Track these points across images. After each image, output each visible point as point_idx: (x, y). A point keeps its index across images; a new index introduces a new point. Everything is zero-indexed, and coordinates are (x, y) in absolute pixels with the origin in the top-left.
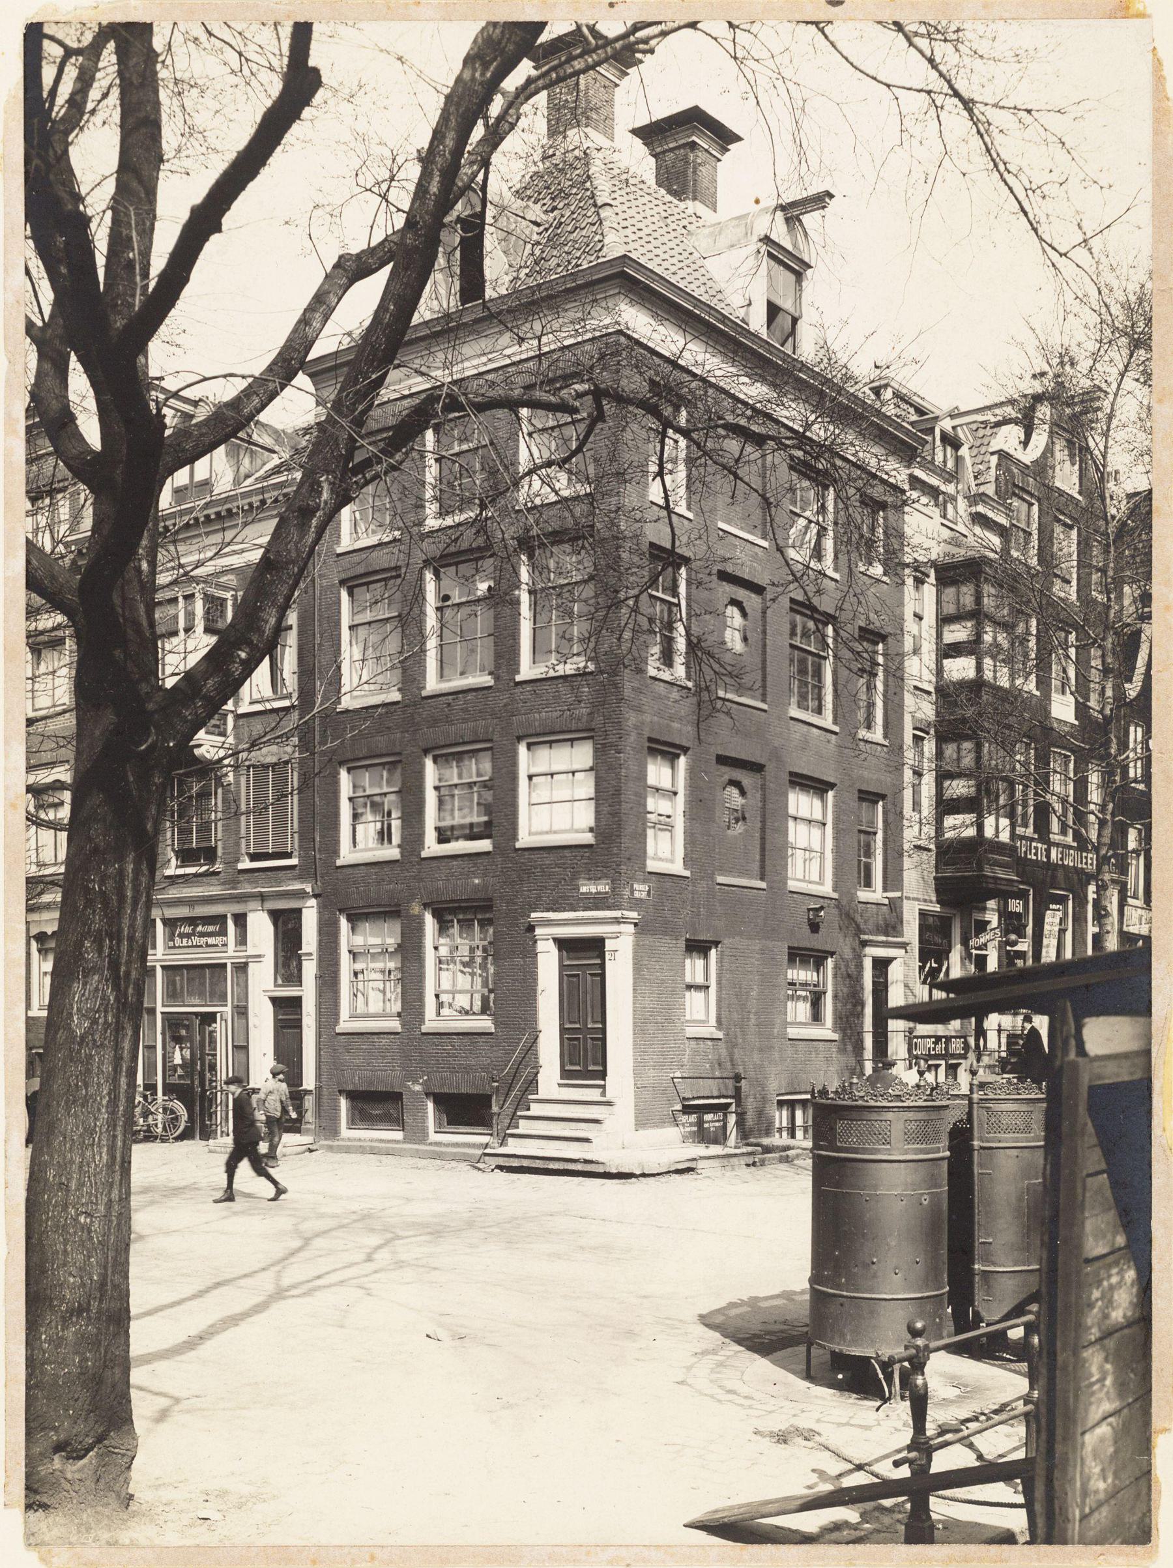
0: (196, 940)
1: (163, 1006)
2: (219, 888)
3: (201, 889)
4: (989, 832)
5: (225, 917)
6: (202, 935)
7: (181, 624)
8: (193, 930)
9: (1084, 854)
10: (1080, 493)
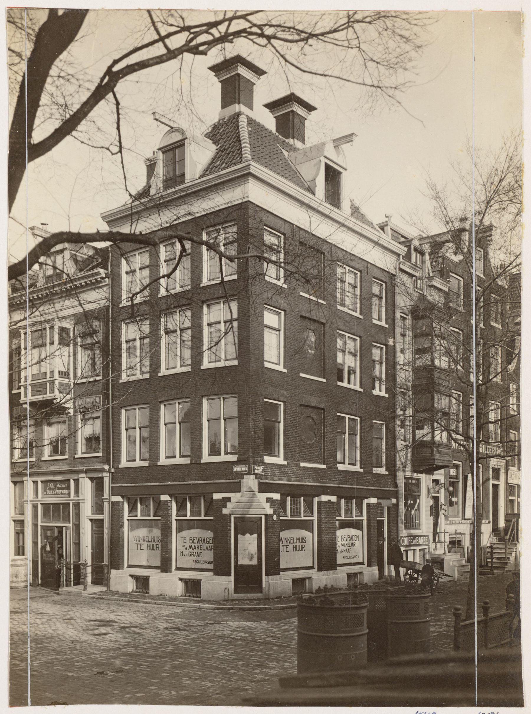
0: (56, 491)
1: (41, 522)
2: (67, 466)
3: (58, 467)
4: (437, 438)
5: (69, 480)
6: (59, 489)
7: (48, 341)
8: (55, 486)
9: (488, 447)
10: (484, 276)
